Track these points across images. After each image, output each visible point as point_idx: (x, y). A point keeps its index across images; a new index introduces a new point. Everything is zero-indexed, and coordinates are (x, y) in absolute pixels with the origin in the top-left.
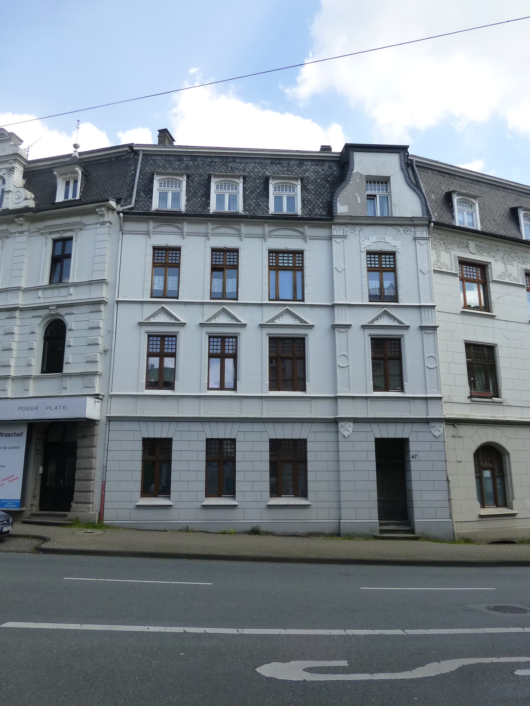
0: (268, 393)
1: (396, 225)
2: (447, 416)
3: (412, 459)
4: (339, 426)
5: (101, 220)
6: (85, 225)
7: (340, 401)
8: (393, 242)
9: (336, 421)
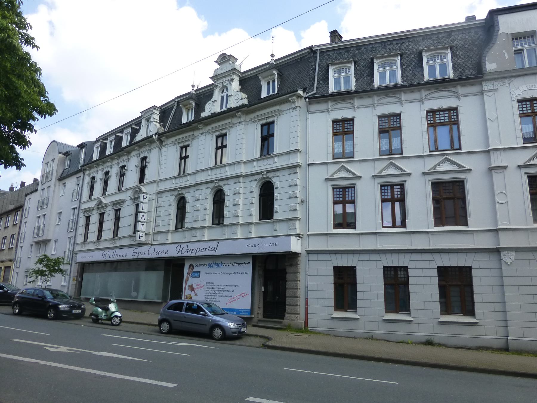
1: (498, 78)
4: (502, 255)
5: (293, 106)
6: (282, 111)
7: (500, 233)
9: (497, 251)
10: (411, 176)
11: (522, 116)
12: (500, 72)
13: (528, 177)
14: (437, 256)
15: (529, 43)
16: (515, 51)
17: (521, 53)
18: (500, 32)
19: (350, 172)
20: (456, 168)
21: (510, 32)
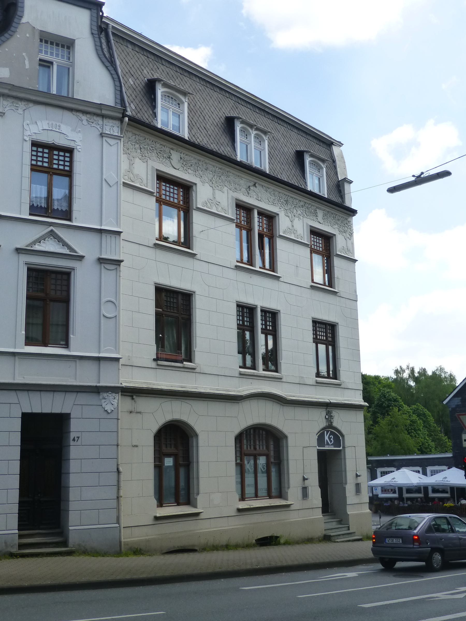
0: (24, 348)
2: (124, 385)
3: (72, 443)
8: (72, 135)
10: (84, 260)
11: (34, 169)
12: (13, 87)
13: (29, 269)
14: (23, 397)
15: (63, 56)
16: (40, 60)
17: (49, 67)
18: (24, 20)
19: (65, 244)
20: (65, 251)
21: (39, 27)
